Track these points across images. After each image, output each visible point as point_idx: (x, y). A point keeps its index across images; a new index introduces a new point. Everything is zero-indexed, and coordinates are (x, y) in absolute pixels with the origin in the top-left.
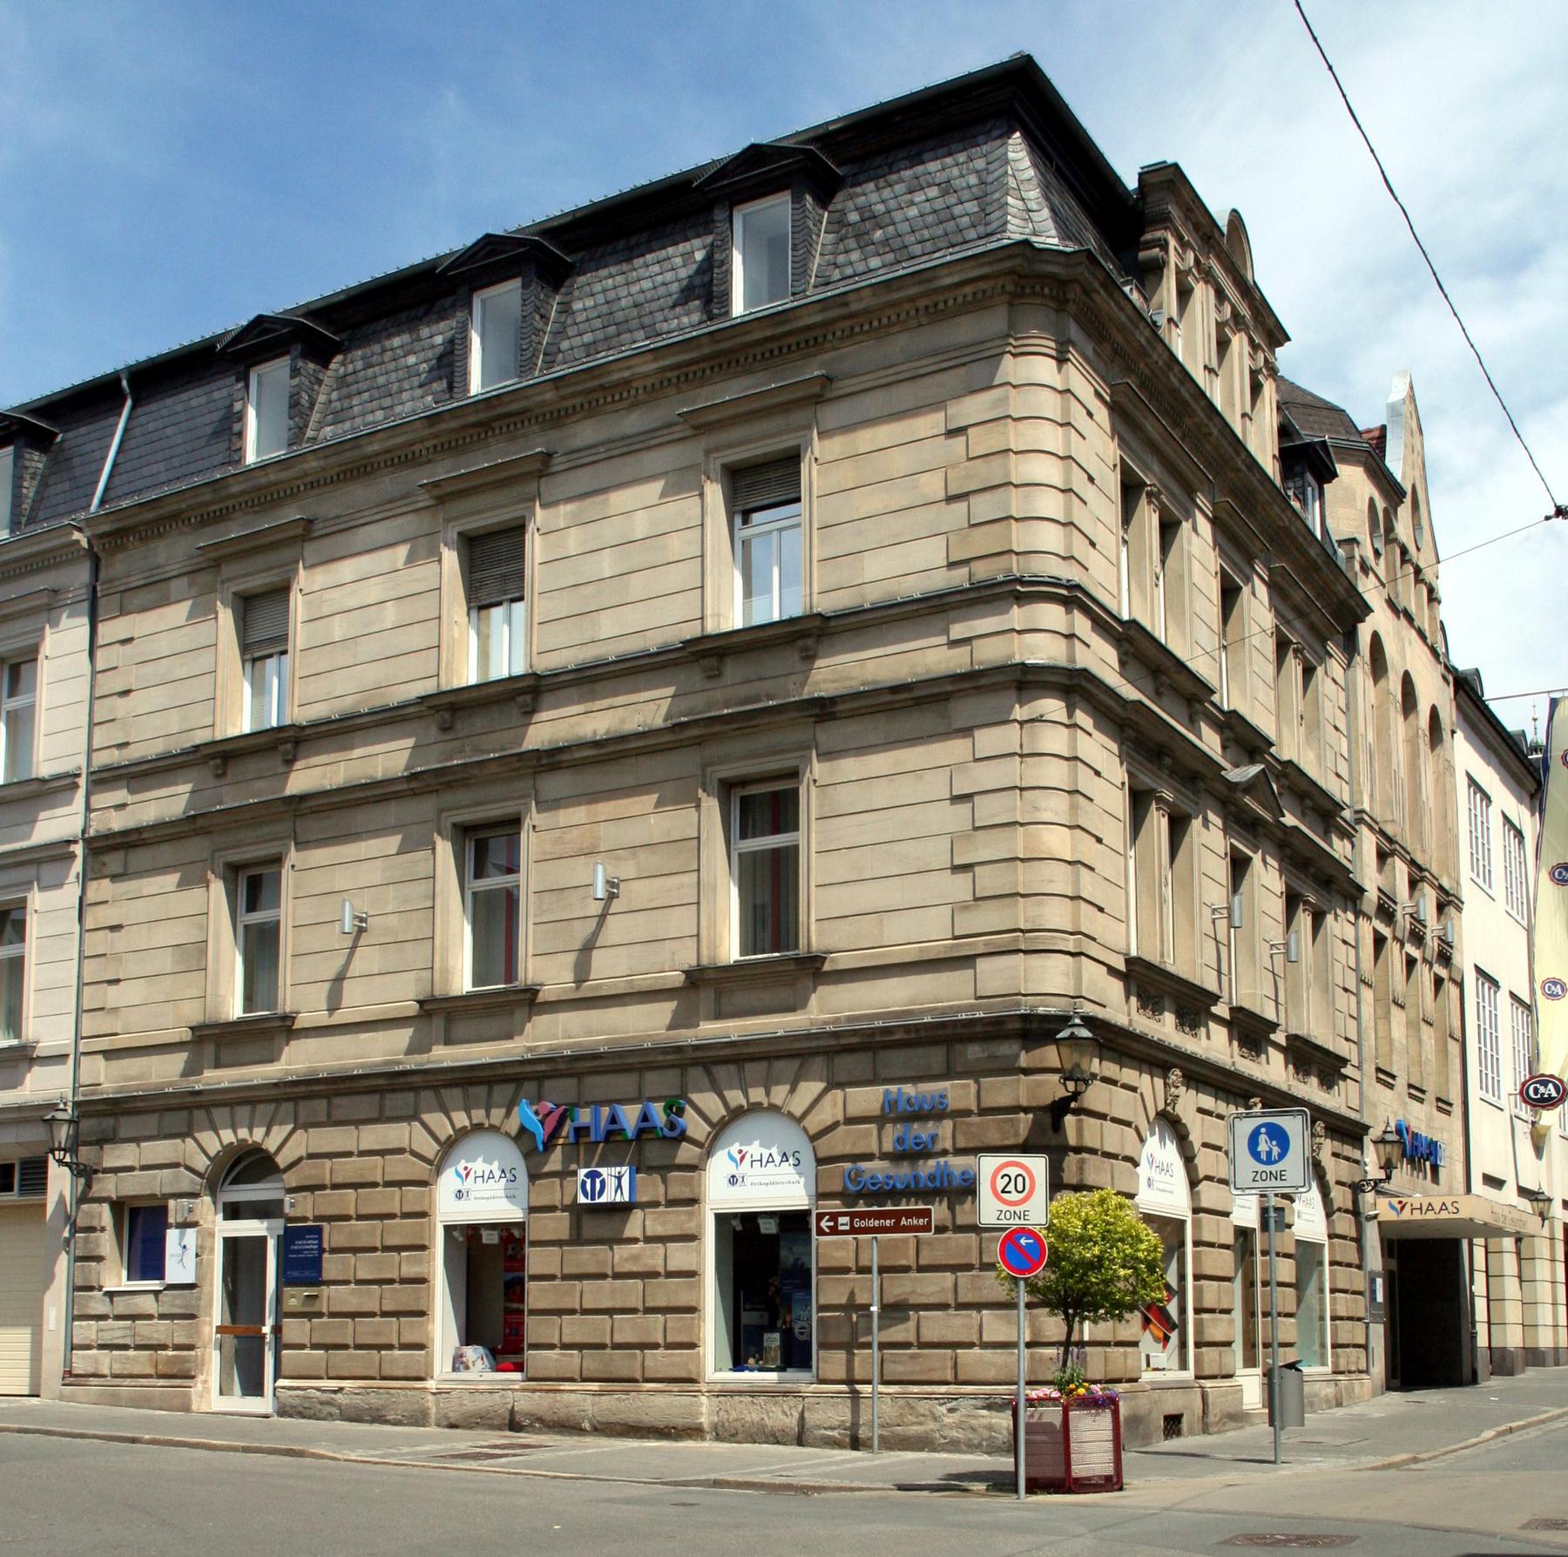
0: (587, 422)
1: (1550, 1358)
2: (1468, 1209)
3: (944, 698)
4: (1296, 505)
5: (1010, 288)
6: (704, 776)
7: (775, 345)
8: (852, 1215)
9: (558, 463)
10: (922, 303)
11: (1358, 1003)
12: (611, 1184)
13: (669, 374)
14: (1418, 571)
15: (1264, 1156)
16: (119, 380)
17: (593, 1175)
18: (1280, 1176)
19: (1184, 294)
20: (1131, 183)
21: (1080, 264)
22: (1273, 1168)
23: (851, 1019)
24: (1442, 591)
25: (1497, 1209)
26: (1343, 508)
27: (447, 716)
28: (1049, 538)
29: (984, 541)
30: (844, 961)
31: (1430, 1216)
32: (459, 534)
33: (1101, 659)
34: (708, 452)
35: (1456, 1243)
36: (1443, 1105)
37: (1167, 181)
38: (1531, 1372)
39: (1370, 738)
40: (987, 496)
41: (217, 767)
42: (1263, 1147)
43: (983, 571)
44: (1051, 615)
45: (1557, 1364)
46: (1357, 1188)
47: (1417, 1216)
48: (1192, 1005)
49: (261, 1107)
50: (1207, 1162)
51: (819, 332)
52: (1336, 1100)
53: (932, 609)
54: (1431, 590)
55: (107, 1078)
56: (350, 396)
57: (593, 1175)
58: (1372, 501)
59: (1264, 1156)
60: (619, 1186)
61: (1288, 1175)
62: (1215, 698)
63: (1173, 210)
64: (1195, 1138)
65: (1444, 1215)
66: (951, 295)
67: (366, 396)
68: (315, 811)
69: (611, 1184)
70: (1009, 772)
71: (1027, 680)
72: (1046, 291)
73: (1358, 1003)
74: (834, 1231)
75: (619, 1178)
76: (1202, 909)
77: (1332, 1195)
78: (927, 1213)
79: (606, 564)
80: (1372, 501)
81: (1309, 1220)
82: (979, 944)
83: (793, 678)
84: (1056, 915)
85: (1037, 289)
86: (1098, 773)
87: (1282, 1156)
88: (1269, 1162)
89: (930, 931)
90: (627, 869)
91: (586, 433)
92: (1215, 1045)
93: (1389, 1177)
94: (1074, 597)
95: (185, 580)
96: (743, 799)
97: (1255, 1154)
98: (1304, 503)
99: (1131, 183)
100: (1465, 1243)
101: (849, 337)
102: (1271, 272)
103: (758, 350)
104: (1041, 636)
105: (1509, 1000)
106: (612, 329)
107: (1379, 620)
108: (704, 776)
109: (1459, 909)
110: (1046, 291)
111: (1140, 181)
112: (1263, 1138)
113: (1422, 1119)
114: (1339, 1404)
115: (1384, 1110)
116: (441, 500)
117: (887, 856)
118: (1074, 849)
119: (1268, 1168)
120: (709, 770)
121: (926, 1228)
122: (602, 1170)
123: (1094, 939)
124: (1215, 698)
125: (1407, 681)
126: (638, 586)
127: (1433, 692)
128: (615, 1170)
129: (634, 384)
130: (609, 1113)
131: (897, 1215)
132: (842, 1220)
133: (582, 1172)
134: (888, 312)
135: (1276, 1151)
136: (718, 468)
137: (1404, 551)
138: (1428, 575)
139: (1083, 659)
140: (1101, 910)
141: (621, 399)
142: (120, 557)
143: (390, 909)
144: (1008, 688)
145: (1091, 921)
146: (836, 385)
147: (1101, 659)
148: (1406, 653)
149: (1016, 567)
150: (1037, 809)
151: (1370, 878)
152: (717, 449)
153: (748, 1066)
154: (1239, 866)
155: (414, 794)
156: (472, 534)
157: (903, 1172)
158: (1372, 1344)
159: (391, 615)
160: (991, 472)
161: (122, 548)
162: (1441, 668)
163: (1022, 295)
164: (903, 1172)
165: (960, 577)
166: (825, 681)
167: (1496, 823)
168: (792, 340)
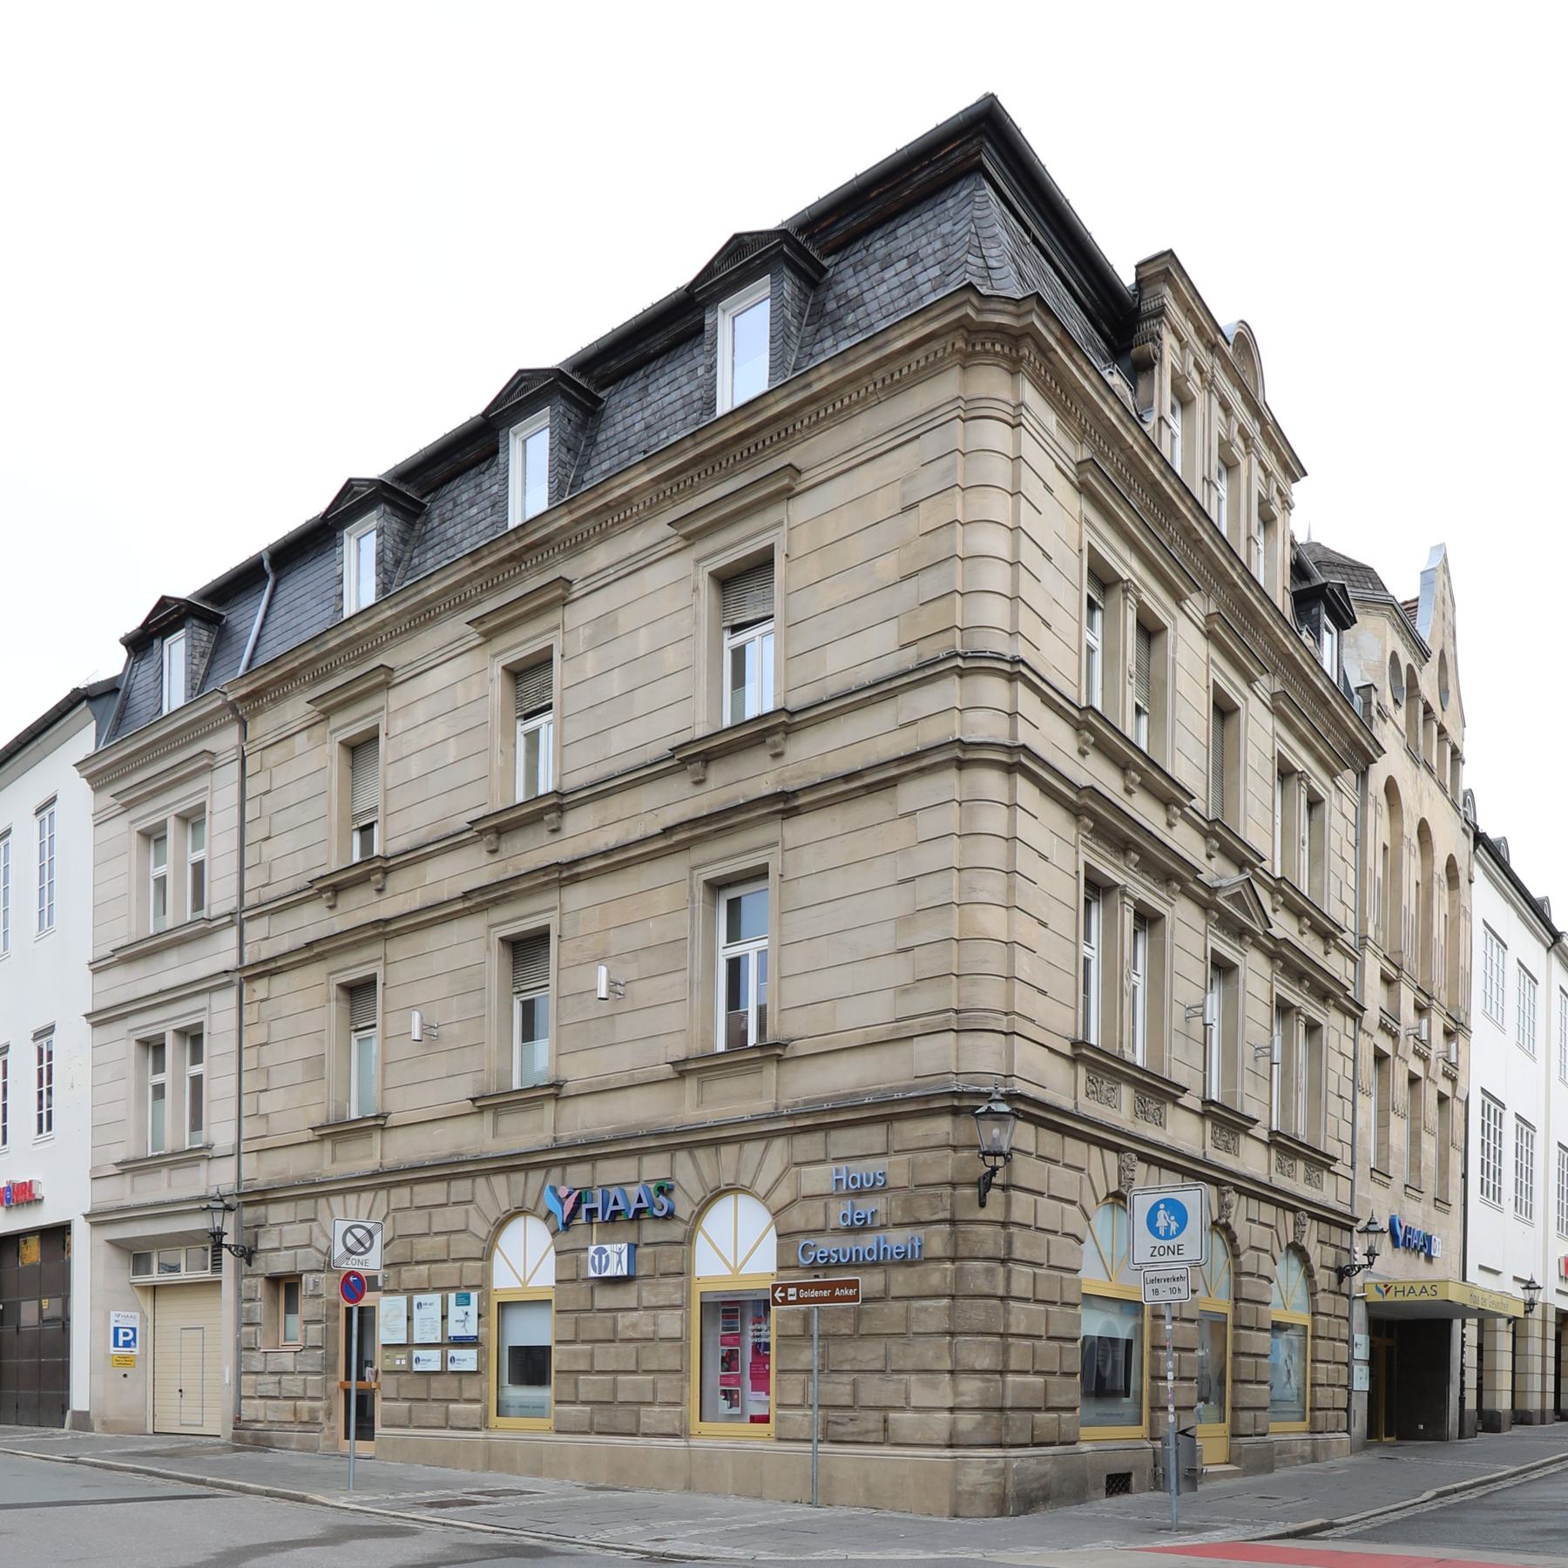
0: (602, 547)
1: (1537, 1418)
2: (1455, 1294)
3: (890, 783)
4: (1309, 642)
5: (960, 344)
6: (691, 878)
7: (749, 442)
8: (799, 1286)
9: (577, 590)
10: (878, 375)
11: (1354, 1110)
12: (614, 1259)
13: (663, 486)
14: (1442, 731)
15: (1162, 1232)
16: (262, 561)
17: (600, 1252)
18: (1178, 1250)
19: (1183, 401)
20: (1127, 278)
21: (1030, 312)
22: (1171, 1243)
23: (806, 1102)
24: (1467, 752)
25: (1478, 1293)
26: (1357, 655)
27: (492, 837)
28: (995, 612)
29: (931, 620)
30: (802, 1048)
31: (1412, 1297)
32: (504, 668)
33: (1053, 739)
34: (698, 561)
35: (1446, 1325)
36: (1441, 1202)
37: (1163, 269)
38: (1518, 1430)
39: (1380, 873)
40: (934, 572)
41: (329, 899)
42: (1161, 1223)
43: (930, 650)
44: (994, 690)
45: (1543, 1423)
46: (1343, 1273)
47: (1400, 1298)
48: (1157, 1091)
49: (364, 1195)
50: (1248, 1260)
51: (788, 422)
52: (1328, 1193)
53: (882, 691)
54: (1455, 752)
55: (259, 1172)
56: (425, 552)
57: (600, 1252)
58: (1394, 656)
59: (1162, 1232)
60: (620, 1261)
61: (1185, 1250)
62: (1266, 865)
63: (1175, 312)
64: (1242, 1241)
65: (1424, 1297)
66: (903, 361)
67: (437, 549)
68: (399, 933)
69: (614, 1259)
70: (950, 853)
71: (962, 756)
72: (998, 348)
73: (1354, 1110)
74: (785, 1301)
75: (620, 1254)
76: (1199, 1016)
77: (1317, 1277)
78: (854, 1284)
79: (615, 684)
80: (1394, 656)
81: (1286, 1296)
82: (917, 1026)
83: (765, 777)
84: (989, 995)
85: (988, 346)
86: (1042, 856)
87: (1180, 1231)
88: (1167, 1237)
89: (877, 1012)
90: (630, 972)
91: (601, 556)
92: (1183, 1132)
93: (1371, 1264)
94: (1015, 671)
95: (304, 734)
96: (730, 902)
97: (1153, 1229)
98: (1318, 640)
99: (1127, 278)
100: (1457, 1323)
101: (816, 423)
102: (1282, 395)
103: (736, 450)
104: (984, 710)
105: (1515, 1121)
106: (626, 454)
107: (1393, 762)
108: (691, 878)
109: (1468, 1038)
110: (998, 348)
111: (1137, 274)
112: (1161, 1213)
113: (1416, 1215)
114: (1315, 1460)
115: (1378, 1204)
116: (489, 636)
117: (841, 944)
118: (1010, 930)
119: (1165, 1243)
120: (696, 872)
121: (855, 1298)
122: (606, 1247)
123: (1033, 1021)
124: (1266, 865)
125: (1423, 829)
126: (642, 701)
127: (1449, 840)
128: (616, 1247)
129: (635, 501)
130: (619, 1199)
131: (832, 1286)
132: (792, 1291)
133: (592, 1249)
134: (848, 390)
135: (1174, 1225)
136: (706, 576)
137: (1428, 710)
138: (1453, 735)
139: (1025, 736)
140: (1044, 993)
141: (626, 519)
142: (260, 718)
143: (454, 1018)
144: (948, 768)
145: (1025, 1001)
146: (805, 476)
147: (1053, 739)
148: (1423, 798)
149: (957, 642)
150: (974, 890)
151: (1374, 997)
152: (705, 558)
153: (724, 1150)
154: (1222, 969)
155: (468, 912)
156: (517, 668)
157: (847, 1244)
158: (1354, 1406)
159: (452, 751)
160: (939, 546)
161: (258, 711)
162: (1460, 823)
163: (974, 354)
164: (847, 1244)
165: (909, 658)
166: (792, 778)
167: (1512, 969)
168: (765, 434)
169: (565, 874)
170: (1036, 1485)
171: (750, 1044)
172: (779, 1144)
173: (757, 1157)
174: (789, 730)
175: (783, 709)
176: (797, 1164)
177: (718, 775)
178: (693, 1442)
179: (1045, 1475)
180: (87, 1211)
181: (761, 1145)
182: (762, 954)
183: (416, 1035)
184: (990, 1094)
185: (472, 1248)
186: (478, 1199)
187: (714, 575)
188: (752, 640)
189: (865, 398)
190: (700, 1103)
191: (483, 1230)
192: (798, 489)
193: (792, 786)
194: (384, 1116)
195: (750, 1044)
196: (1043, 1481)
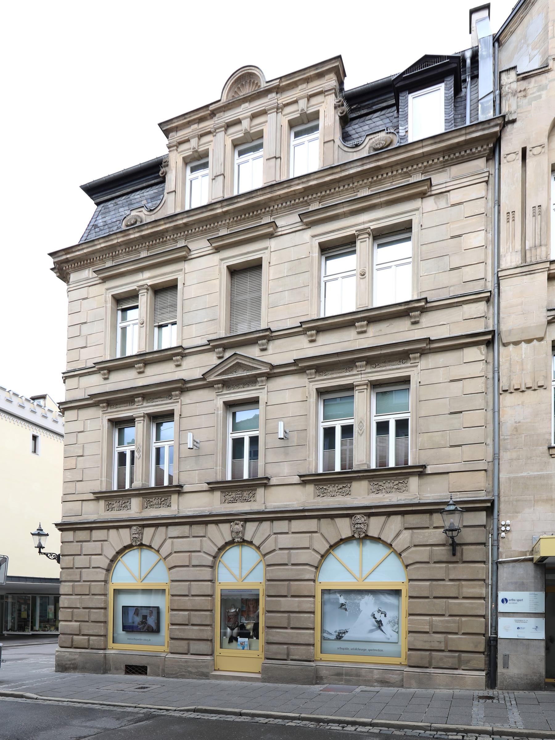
32: (113, 296)
146: (280, 229)
156: (118, 297)
169: (427, 348)
170: (69, 663)
171: (127, 488)
172: (162, 529)
173: (254, 529)
174: (423, 310)
175: (181, 346)
176: (275, 534)
177: (373, 330)
178: (108, 652)
179: (75, 659)
180: (59, 521)
181: (256, 524)
182: (133, 452)
183: (281, 435)
184: (449, 502)
185: (313, 558)
186: (110, 539)
187: (228, 267)
188: (129, 325)
189: (118, 255)
190: (144, 508)
191: (323, 547)
192: (190, 257)
193: (187, 378)
194: (424, 467)
195: (127, 488)
196: (73, 662)
